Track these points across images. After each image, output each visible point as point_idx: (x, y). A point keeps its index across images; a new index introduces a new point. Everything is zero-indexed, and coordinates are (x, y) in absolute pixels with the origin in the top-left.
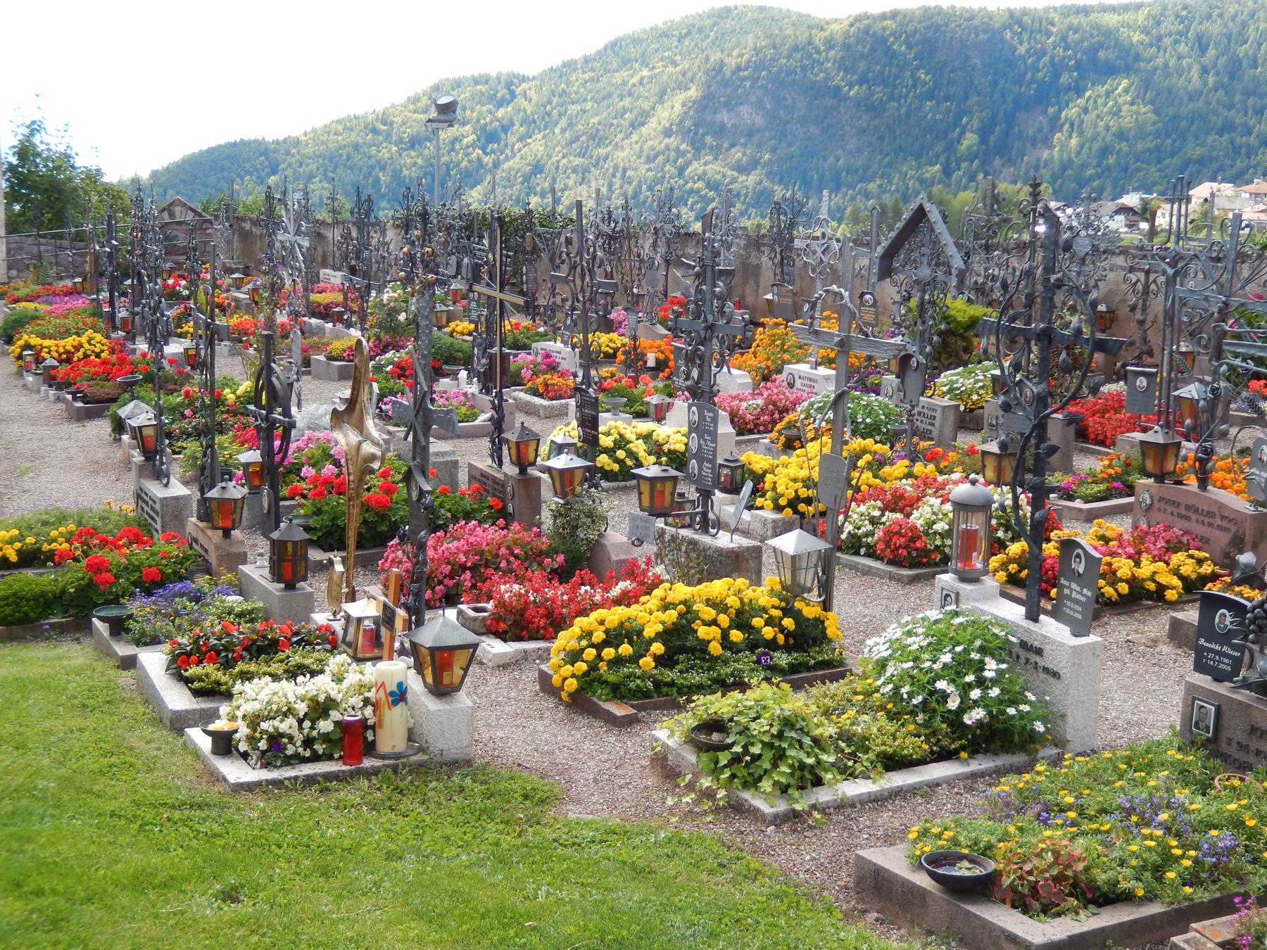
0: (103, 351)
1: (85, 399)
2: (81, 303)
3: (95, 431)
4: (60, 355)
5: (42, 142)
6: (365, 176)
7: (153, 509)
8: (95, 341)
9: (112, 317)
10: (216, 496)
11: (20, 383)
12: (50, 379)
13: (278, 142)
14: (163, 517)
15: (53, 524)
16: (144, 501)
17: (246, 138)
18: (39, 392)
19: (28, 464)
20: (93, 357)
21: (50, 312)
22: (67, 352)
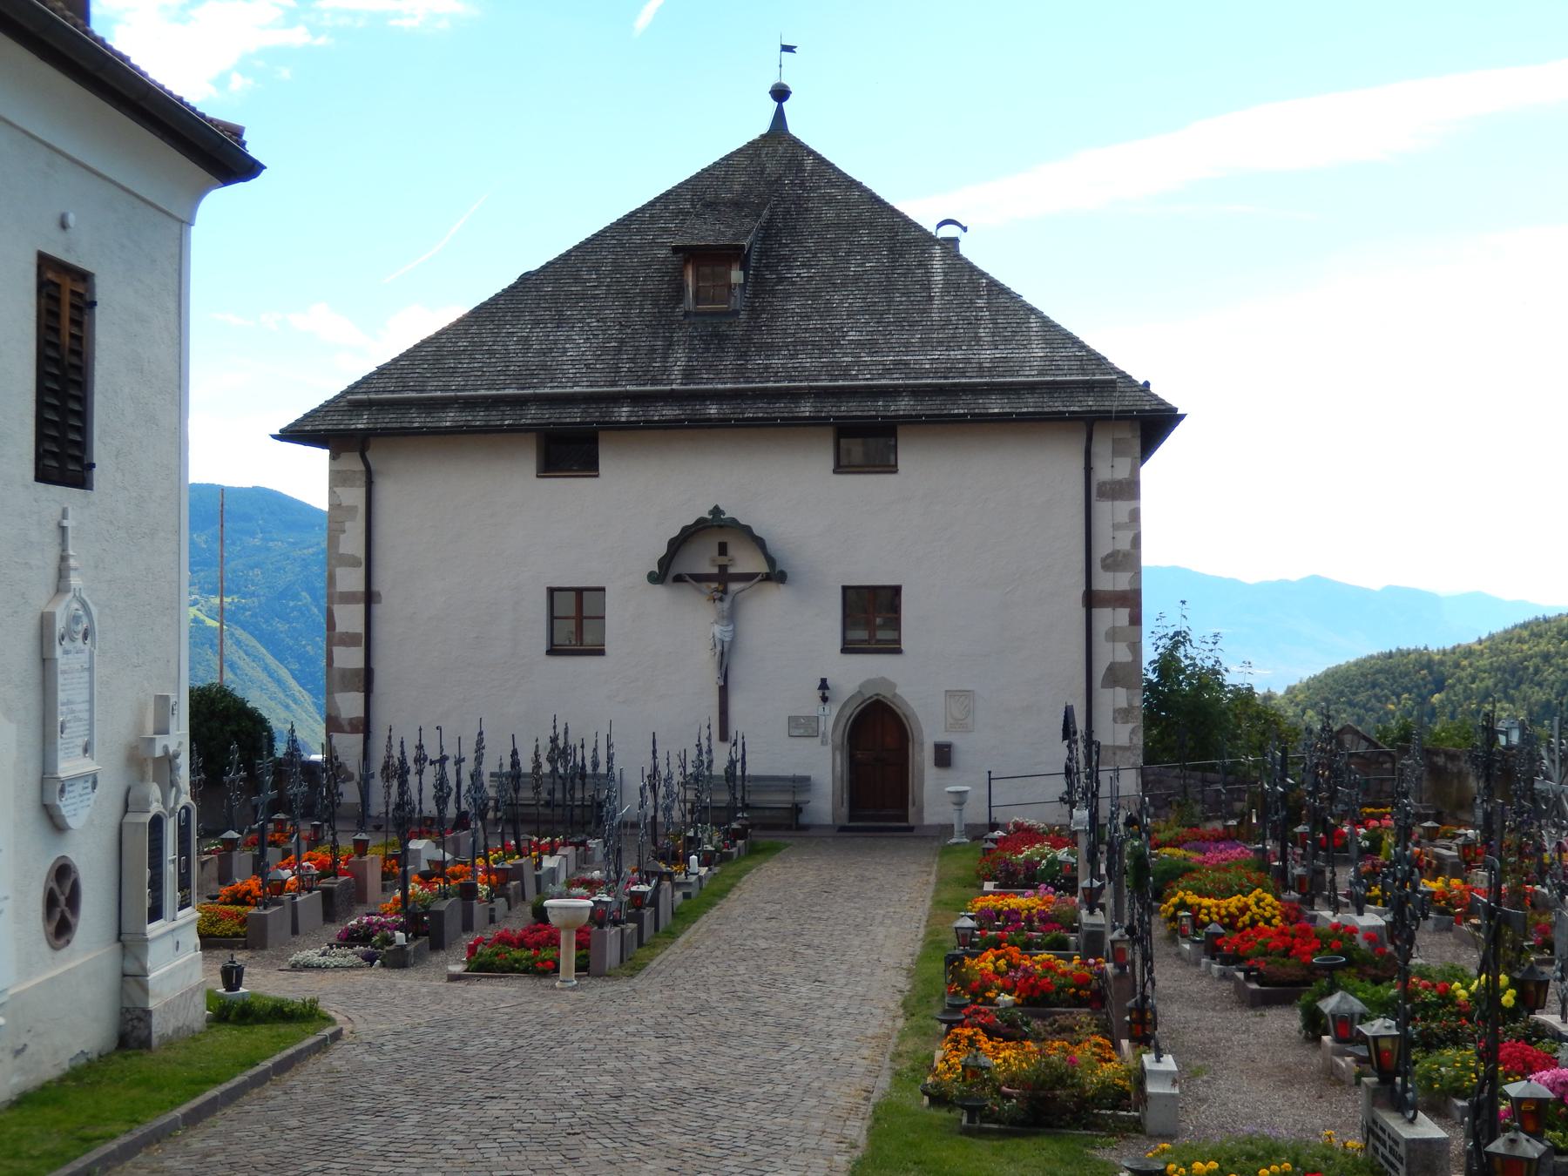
0: (1274, 916)
1: (1259, 979)
2: (1243, 852)
3: (1277, 1025)
4: (1221, 918)
5: (1186, 656)
6: (1558, 695)
7: (1391, 1151)
8: (1264, 903)
9: (1282, 873)
10: (1502, 1150)
11: (1173, 950)
12: (1212, 948)
13: (1444, 653)
14: (1408, 1166)
15: (1261, 1159)
16: (1378, 1138)
17: (1404, 647)
18: (1198, 964)
19: (1199, 1063)
20: (1261, 924)
21: (1203, 863)
22: (1230, 915)
